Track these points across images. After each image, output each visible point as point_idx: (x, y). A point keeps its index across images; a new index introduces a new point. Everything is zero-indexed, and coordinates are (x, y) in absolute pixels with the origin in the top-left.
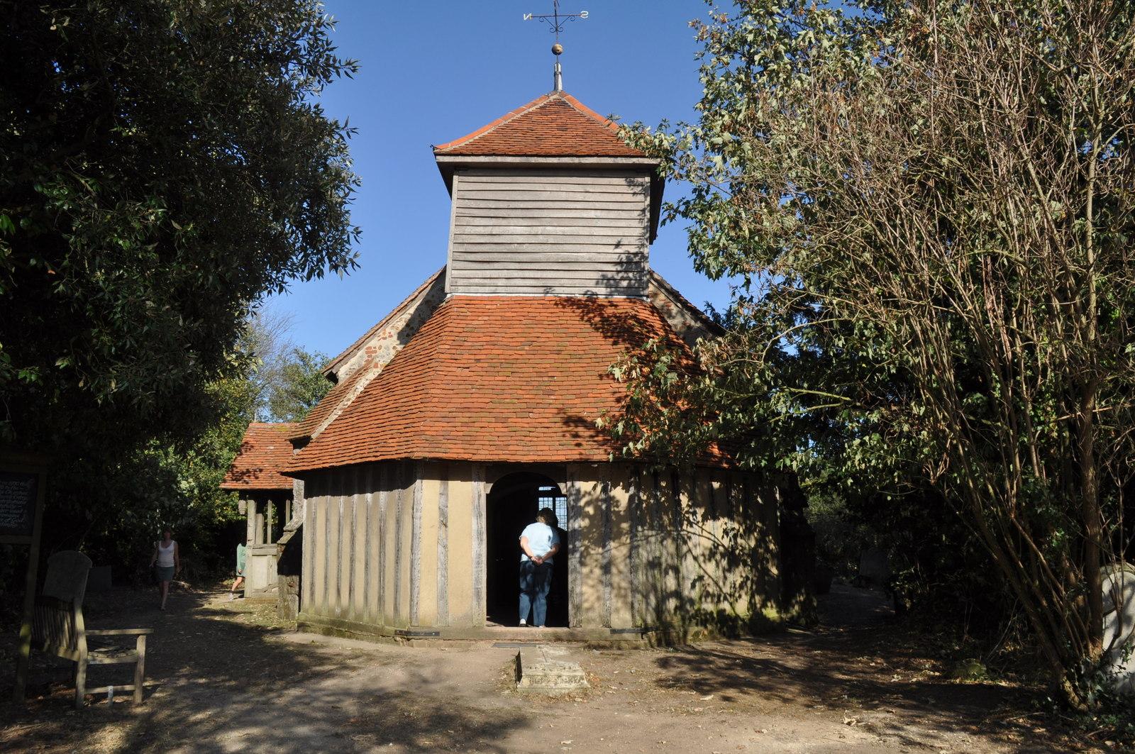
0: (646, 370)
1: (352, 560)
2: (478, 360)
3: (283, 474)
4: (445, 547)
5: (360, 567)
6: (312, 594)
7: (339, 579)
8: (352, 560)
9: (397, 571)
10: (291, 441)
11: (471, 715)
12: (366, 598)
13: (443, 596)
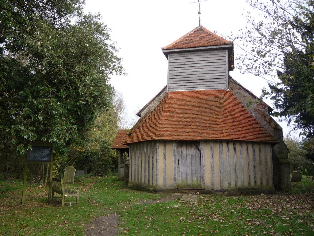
1: (141, 169)
3: (124, 144)
4: (165, 165)
8: (141, 169)
10: (128, 134)
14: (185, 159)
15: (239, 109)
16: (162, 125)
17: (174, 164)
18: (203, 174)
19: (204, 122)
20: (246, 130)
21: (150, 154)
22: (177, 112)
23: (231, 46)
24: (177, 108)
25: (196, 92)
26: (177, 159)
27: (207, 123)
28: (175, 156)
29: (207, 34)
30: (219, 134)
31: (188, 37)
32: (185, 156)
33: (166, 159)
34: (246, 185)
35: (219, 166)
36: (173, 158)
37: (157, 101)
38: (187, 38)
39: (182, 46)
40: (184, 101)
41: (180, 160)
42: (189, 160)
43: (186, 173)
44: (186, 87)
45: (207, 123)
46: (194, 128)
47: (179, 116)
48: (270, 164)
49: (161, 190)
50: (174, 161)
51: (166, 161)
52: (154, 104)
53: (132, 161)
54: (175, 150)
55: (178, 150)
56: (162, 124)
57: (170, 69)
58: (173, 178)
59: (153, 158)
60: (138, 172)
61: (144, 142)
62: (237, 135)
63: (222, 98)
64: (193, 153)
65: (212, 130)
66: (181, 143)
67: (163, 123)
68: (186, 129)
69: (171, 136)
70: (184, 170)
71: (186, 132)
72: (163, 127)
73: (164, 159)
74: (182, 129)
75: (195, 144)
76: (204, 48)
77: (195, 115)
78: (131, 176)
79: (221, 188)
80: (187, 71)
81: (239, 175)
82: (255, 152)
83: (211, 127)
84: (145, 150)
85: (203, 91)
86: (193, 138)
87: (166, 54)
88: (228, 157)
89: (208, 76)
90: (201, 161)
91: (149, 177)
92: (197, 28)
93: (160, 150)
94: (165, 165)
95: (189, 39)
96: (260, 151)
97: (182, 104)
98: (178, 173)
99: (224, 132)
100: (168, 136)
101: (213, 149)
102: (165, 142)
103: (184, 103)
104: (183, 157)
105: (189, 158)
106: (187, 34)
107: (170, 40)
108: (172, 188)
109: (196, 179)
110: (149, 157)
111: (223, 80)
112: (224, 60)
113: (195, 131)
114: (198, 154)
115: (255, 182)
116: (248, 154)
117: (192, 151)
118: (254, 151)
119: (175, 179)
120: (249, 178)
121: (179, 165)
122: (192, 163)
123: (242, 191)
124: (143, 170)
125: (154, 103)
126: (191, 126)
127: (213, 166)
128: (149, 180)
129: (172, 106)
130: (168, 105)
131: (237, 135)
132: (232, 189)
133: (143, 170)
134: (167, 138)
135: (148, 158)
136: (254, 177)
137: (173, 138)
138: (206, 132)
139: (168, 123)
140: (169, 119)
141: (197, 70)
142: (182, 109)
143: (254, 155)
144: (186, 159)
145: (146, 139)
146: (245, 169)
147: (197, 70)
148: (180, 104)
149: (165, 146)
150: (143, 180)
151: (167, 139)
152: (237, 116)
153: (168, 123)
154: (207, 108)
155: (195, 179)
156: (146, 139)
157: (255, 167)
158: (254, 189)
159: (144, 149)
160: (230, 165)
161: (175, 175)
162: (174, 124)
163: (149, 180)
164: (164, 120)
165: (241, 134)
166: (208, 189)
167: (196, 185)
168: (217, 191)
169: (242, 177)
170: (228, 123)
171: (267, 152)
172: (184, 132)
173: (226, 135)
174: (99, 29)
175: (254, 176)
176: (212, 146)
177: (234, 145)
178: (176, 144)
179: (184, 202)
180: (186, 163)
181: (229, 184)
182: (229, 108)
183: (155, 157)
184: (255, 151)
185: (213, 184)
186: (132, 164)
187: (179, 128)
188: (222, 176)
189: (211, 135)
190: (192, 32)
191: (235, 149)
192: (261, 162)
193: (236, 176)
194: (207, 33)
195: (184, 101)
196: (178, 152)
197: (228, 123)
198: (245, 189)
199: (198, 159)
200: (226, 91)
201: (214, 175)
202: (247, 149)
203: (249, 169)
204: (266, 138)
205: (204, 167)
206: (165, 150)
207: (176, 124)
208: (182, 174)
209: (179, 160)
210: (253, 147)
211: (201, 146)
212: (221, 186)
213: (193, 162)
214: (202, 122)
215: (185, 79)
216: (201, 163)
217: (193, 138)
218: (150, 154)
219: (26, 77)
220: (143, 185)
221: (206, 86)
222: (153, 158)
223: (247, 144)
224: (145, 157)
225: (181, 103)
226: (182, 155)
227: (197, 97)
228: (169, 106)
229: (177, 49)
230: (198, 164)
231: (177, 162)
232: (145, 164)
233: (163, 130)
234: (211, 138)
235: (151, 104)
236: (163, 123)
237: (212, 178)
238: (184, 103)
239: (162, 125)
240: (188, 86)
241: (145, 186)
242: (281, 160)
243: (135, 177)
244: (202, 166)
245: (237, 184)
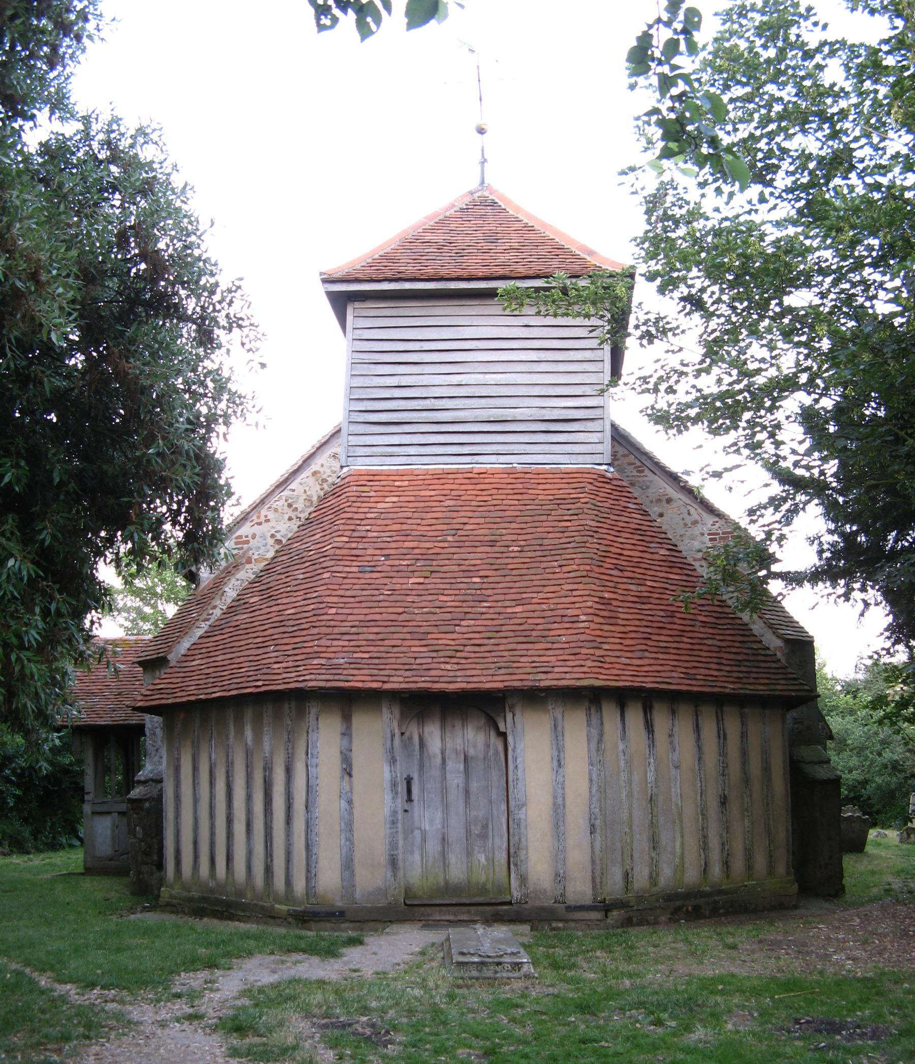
1: (230, 820)
3: (135, 709)
8: (230, 820)
10: (141, 663)
14: (436, 772)
15: (656, 557)
16: (332, 623)
17: (388, 797)
18: (517, 838)
19: (519, 609)
20: (690, 646)
21: (272, 753)
22: (396, 563)
24: (393, 545)
25: (474, 478)
26: (401, 771)
27: (532, 614)
28: (393, 761)
29: (517, 225)
30: (589, 663)
31: (432, 230)
32: (439, 760)
33: (350, 775)
34: (692, 876)
35: (562, 797)
36: (386, 769)
37: (276, 510)
38: (429, 236)
39: (411, 269)
40: (424, 515)
41: (416, 776)
42: (455, 779)
43: (440, 837)
45: (532, 614)
46: (477, 636)
47: (405, 581)
48: (780, 785)
49: (332, 914)
50: (387, 785)
51: (351, 783)
52: (260, 524)
53: (177, 786)
54: (393, 736)
55: (407, 734)
56: (330, 617)
58: (383, 859)
59: (289, 771)
60: (213, 834)
61: (240, 702)
62: (660, 668)
63: (589, 506)
64: (475, 746)
65: (555, 646)
66: (424, 704)
67: (333, 611)
68: (440, 642)
69: (376, 672)
70: (432, 821)
71: (441, 654)
72: (336, 630)
73: (342, 778)
74: (424, 642)
75: (486, 706)
77: (475, 580)
78: (178, 852)
79: (595, 895)
80: (433, 381)
81: (664, 838)
82: (725, 738)
83: (552, 633)
84: (249, 733)
86: (475, 679)
87: (341, 302)
88: (622, 763)
89: (526, 409)
90: (510, 783)
91: (271, 856)
92: (471, 193)
93: (325, 736)
94: (350, 802)
95: (440, 238)
96: (744, 735)
97: (415, 527)
98: (405, 839)
99: (610, 653)
100: (362, 672)
101: (560, 728)
102: (347, 701)
103: (424, 522)
104: (427, 764)
105: (455, 766)
106: (428, 218)
107: (364, 236)
108: (382, 903)
109: (487, 859)
110: (268, 769)
111: (590, 426)
113: (483, 649)
114: (496, 753)
115: (726, 865)
116: (700, 748)
117: (471, 737)
118: (722, 736)
119: (393, 862)
120: (704, 846)
121: (410, 800)
122: (467, 792)
123: (678, 903)
124: (239, 828)
125: (262, 519)
126: (464, 630)
127: (560, 801)
128: (268, 870)
129: (370, 534)
130: (348, 533)
131: (660, 668)
132: (640, 898)
133: (239, 828)
134: (360, 680)
135: (265, 769)
136: (723, 844)
137: (386, 679)
138: (530, 653)
139: (355, 611)
140: (360, 593)
142: (416, 551)
143: (723, 752)
144: (444, 778)
145: (260, 683)
146: (690, 810)
148: (405, 527)
149: (347, 718)
150: (243, 866)
151: (360, 685)
152: (654, 584)
153: (355, 611)
154: (526, 549)
155: (482, 858)
156: (260, 683)
157: (724, 801)
158: (720, 892)
159: (240, 731)
160: (630, 795)
161: (393, 845)
162: (385, 617)
163: (268, 870)
164: (335, 599)
165: (675, 663)
166: (537, 903)
167: (489, 886)
168: (582, 908)
169: (678, 844)
170: (622, 616)
171: (768, 736)
172: (434, 654)
173: (617, 666)
174: (141, 182)
175: (721, 836)
176: (559, 717)
177: (647, 710)
178: (397, 711)
179: (476, 959)
180: (444, 791)
181: (626, 875)
182: (619, 551)
184: (725, 735)
185: (560, 878)
186: (177, 798)
187: (408, 636)
188: (598, 844)
189: (556, 670)
190: (452, 211)
191: (649, 727)
192: (746, 780)
193: (655, 843)
195: (424, 515)
196: (407, 744)
197: (622, 616)
198: (690, 894)
199: (496, 776)
200: (604, 477)
201: (564, 840)
202: (697, 729)
203: (702, 810)
204: (767, 681)
205: (523, 805)
206: (347, 733)
207: (393, 617)
208: (424, 840)
209: (409, 781)
210: (719, 720)
211: (509, 716)
212: (594, 888)
213: (474, 785)
214: (509, 610)
215: (425, 414)
216: (510, 791)
217: (475, 679)
218: (272, 753)
219: (841, 499)
220: (240, 893)
222: (289, 771)
223: (696, 707)
225: (409, 521)
226: (425, 755)
227: (479, 498)
228: (356, 534)
229: (391, 280)
230: (496, 793)
231: (402, 788)
232: (249, 798)
233: (335, 643)
234: (555, 683)
235: (248, 524)
236: (333, 611)
237: (559, 855)
238: (424, 522)
239: (332, 623)
241: (249, 895)
242: (808, 769)
243: (196, 857)
244: (512, 803)
245: (658, 875)
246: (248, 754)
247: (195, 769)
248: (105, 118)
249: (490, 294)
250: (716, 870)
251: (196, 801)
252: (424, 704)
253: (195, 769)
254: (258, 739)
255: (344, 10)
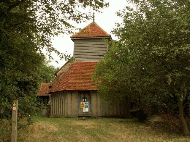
0: (121, 30)
1: (58, 107)
2: (78, 74)
3: (48, 93)
4: (72, 104)
5: (59, 108)
6: (52, 113)
7: (56, 110)
8: (58, 107)
9: (65, 108)
10: (49, 87)
11: (117, 41)
12: (60, 112)
13: (72, 112)
23: (110, 37)
44: (84, 60)
57: (74, 45)
59: (65, 100)
76: (95, 38)
85: (94, 62)
89: (97, 54)
93: (69, 97)
94: (72, 104)
110: (63, 100)
112: (106, 45)
115: (120, 112)
128: (63, 113)
141: (90, 50)
147: (90, 50)
157: (120, 105)
163: (63, 113)
183: (66, 100)
194: (97, 27)
221: (95, 59)
224: (61, 100)
240: (85, 59)
246: (60, 98)
247: (54, 101)
248: (104, 8)
249: (101, 38)
250: (119, 113)
251: (54, 105)
252: (80, 92)
253: (54, 101)
254: (62, 96)
255: (81, 2)
